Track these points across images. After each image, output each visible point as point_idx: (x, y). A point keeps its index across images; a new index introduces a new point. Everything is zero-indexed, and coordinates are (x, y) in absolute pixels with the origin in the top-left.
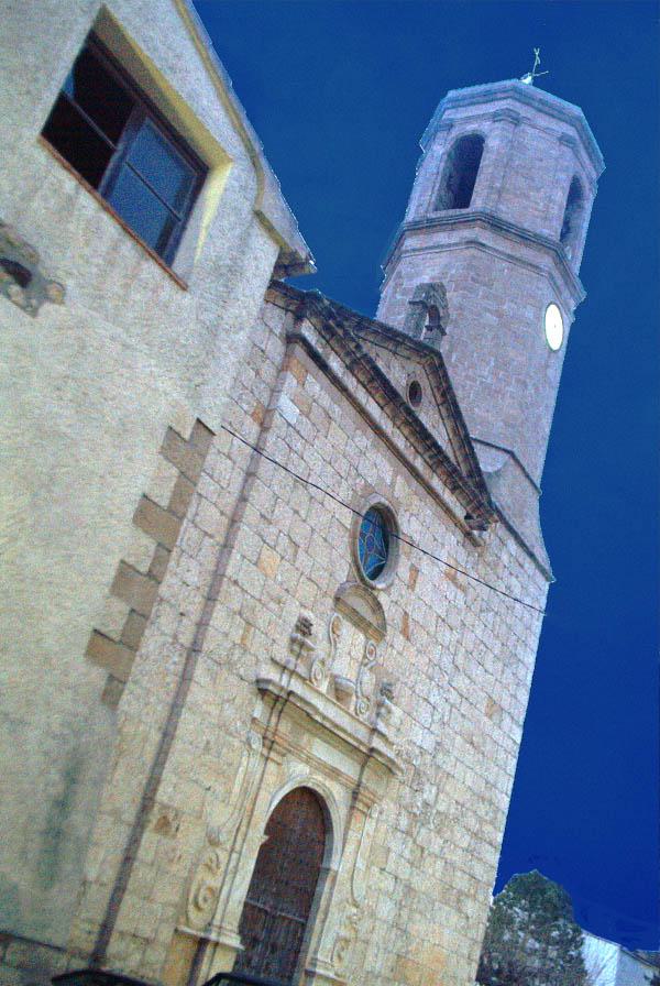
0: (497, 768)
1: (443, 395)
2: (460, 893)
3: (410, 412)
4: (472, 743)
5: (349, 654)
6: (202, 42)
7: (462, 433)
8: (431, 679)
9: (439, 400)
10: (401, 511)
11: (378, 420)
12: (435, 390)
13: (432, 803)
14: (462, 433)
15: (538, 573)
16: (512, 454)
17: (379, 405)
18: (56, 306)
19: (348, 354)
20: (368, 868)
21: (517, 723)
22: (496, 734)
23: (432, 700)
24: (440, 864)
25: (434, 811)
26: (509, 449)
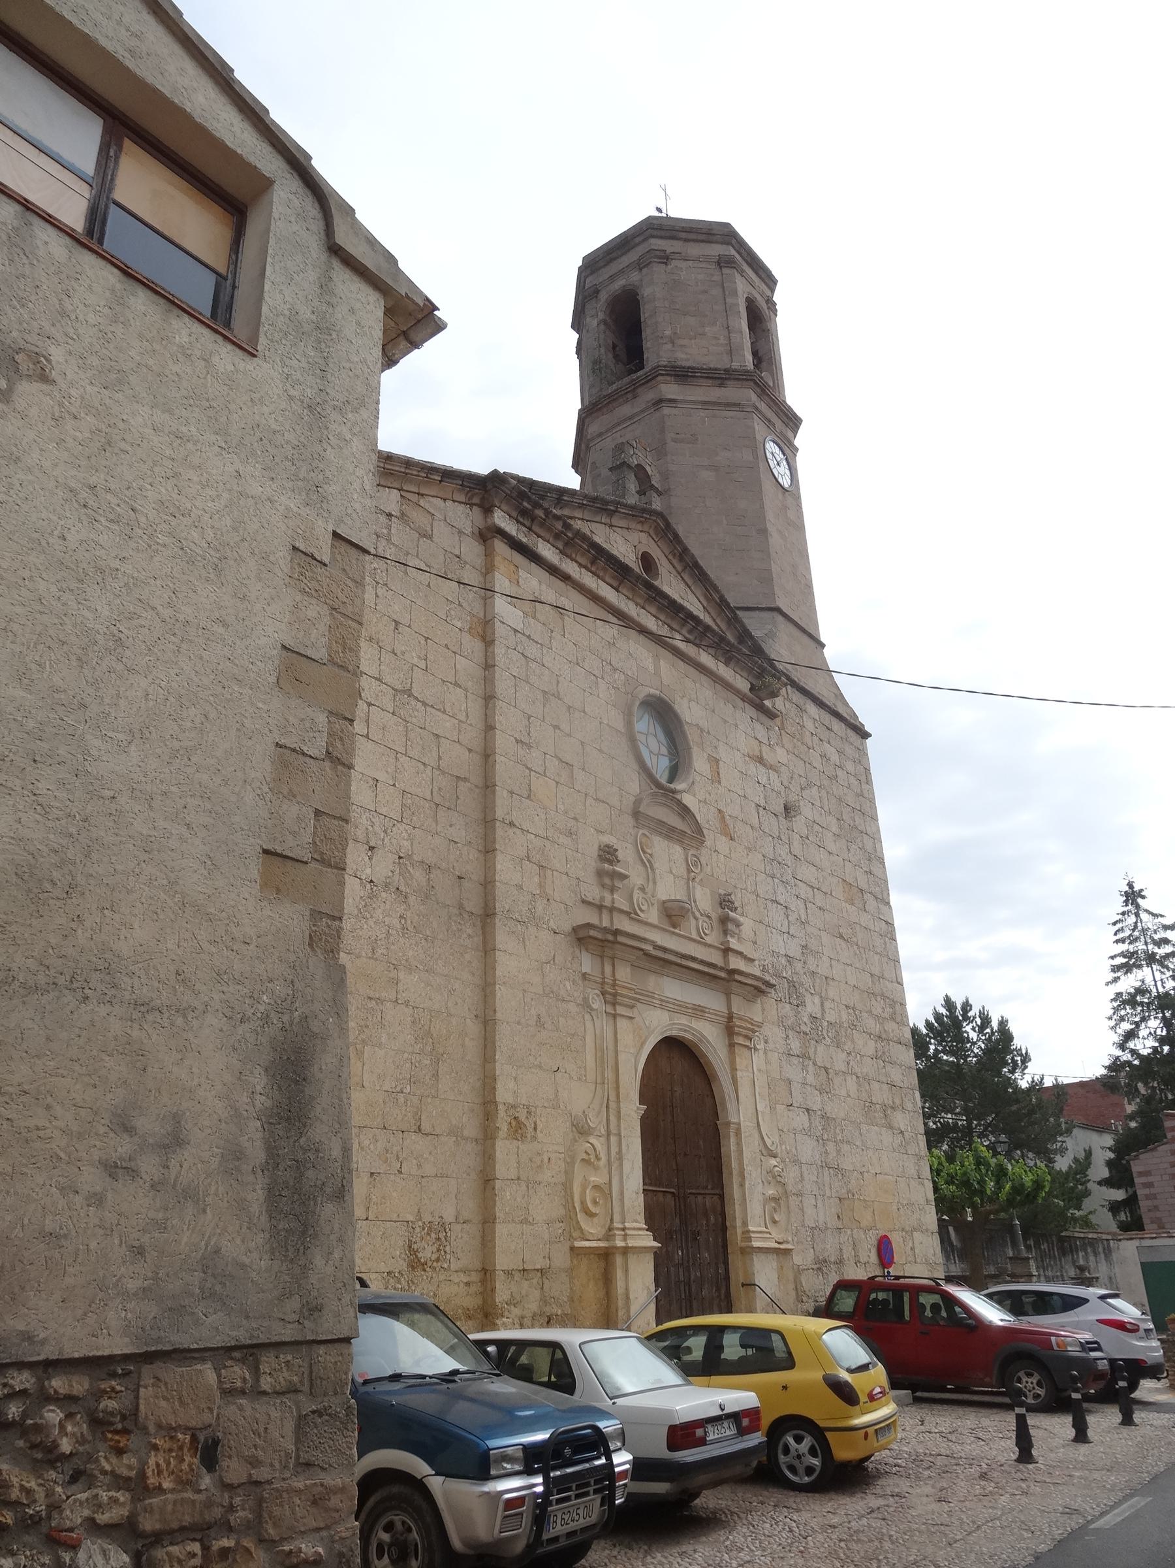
3: (649, 586)
4: (841, 937)
5: (671, 872)
11: (596, 590)
17: (612, 586)
23: (781, 899)
24: (851, 1082)
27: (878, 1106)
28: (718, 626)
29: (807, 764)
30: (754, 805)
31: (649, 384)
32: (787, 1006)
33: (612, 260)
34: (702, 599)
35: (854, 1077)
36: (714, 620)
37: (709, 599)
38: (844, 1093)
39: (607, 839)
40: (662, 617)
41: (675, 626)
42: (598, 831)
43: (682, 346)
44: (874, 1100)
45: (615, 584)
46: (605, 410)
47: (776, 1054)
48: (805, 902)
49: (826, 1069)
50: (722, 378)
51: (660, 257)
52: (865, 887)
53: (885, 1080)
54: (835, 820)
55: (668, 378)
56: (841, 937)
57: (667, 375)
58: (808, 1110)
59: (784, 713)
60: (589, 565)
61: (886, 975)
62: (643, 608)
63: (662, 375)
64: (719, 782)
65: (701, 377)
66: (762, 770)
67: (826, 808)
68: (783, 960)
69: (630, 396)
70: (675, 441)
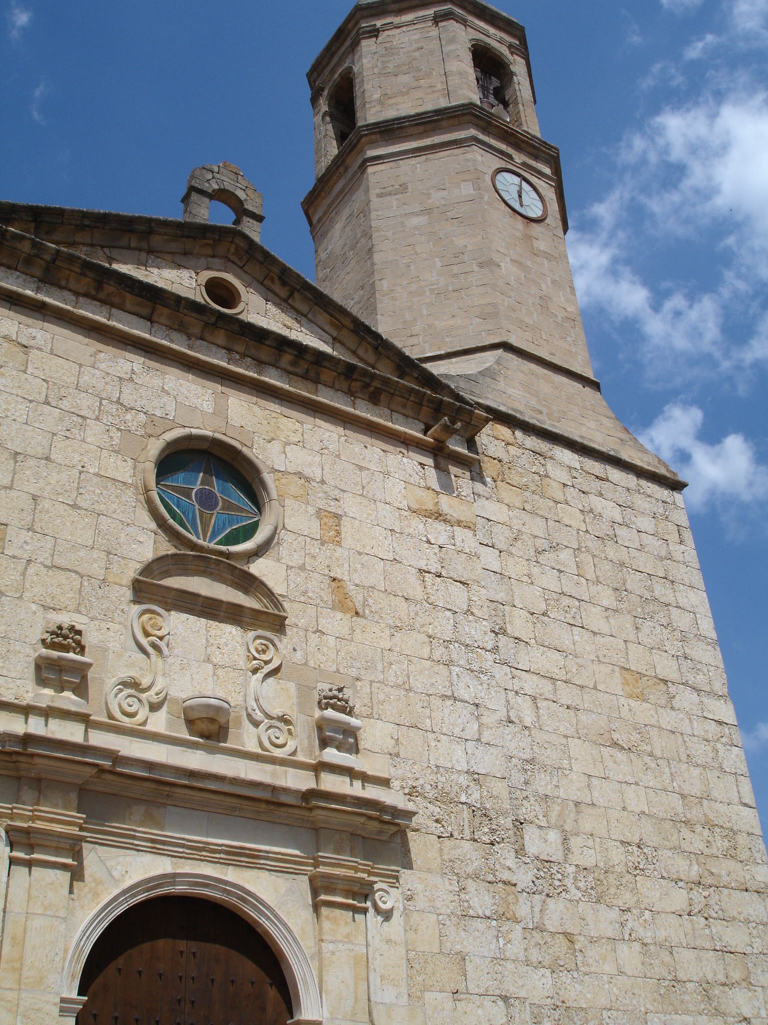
0: (696, 772)
1: (284, 284)
2: (706, 987)
3: (234, 320)
4: (615, 744)
5: (208, 660)
6: (404, 102)
7: (347, 322)
8: (449, 664)
9: (284, 293)
10: (259, 442)
11: (608, 467)
12: (267, 282)
13: (558, 856)
14: (347, 322)
15: (643, 483)
16: (506, 346)
17: (141, 317)
18: (574, 811)
19: (29, 261)
20: (415, 997)
21: (711, 693)
22: (668, 719)
23: (462, 693)
24: (629, 955)
25: (572, 869)
26: (497, 340)
27: (689, 985)
28: (361, 359)
29: (551, 523)
30: (414, 571)
31: (355, 151)
32: (467, 845)
33: (332, 56)
34: (327, 328)
35: (637, 946)
36: (354, 353)
37: (340, 327)
38: (609, 968)
39: (65, 619)
40: (241, 348)
41: (264, 357)
42: (46, 608)
43: (391, 105)
44: (681, 976)
45: (146, 311)
46: (323, 194)
47: (433, 918)
48: (534, 699)
49: (569, 937)
50: (435, 121)
51: (370, 32)
52: (673, 676)
53: (708, 945)
54: (610, 592)
55: (374, 137)
56: (615, 744)
57: (372, 134)
58: (505, 999)
59: (505, 460)
60: (93, 292)
61: (715, 794)
62: (202, 339)
63: (365, 135)
64: (339, 543)
65: (411, 126)
66: (440, 526)
67: (590, 575)
68: (463, 780)
69: (341, 170)
70: (380, 196)
